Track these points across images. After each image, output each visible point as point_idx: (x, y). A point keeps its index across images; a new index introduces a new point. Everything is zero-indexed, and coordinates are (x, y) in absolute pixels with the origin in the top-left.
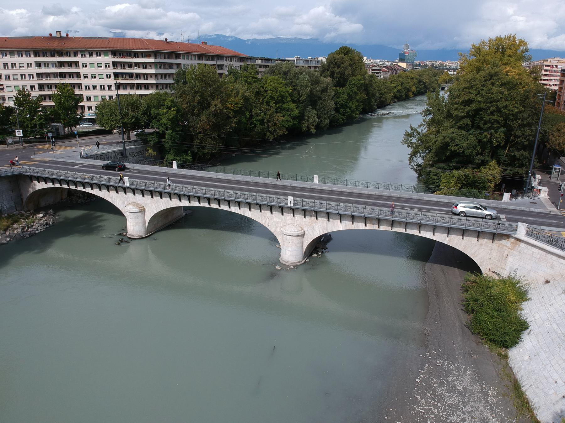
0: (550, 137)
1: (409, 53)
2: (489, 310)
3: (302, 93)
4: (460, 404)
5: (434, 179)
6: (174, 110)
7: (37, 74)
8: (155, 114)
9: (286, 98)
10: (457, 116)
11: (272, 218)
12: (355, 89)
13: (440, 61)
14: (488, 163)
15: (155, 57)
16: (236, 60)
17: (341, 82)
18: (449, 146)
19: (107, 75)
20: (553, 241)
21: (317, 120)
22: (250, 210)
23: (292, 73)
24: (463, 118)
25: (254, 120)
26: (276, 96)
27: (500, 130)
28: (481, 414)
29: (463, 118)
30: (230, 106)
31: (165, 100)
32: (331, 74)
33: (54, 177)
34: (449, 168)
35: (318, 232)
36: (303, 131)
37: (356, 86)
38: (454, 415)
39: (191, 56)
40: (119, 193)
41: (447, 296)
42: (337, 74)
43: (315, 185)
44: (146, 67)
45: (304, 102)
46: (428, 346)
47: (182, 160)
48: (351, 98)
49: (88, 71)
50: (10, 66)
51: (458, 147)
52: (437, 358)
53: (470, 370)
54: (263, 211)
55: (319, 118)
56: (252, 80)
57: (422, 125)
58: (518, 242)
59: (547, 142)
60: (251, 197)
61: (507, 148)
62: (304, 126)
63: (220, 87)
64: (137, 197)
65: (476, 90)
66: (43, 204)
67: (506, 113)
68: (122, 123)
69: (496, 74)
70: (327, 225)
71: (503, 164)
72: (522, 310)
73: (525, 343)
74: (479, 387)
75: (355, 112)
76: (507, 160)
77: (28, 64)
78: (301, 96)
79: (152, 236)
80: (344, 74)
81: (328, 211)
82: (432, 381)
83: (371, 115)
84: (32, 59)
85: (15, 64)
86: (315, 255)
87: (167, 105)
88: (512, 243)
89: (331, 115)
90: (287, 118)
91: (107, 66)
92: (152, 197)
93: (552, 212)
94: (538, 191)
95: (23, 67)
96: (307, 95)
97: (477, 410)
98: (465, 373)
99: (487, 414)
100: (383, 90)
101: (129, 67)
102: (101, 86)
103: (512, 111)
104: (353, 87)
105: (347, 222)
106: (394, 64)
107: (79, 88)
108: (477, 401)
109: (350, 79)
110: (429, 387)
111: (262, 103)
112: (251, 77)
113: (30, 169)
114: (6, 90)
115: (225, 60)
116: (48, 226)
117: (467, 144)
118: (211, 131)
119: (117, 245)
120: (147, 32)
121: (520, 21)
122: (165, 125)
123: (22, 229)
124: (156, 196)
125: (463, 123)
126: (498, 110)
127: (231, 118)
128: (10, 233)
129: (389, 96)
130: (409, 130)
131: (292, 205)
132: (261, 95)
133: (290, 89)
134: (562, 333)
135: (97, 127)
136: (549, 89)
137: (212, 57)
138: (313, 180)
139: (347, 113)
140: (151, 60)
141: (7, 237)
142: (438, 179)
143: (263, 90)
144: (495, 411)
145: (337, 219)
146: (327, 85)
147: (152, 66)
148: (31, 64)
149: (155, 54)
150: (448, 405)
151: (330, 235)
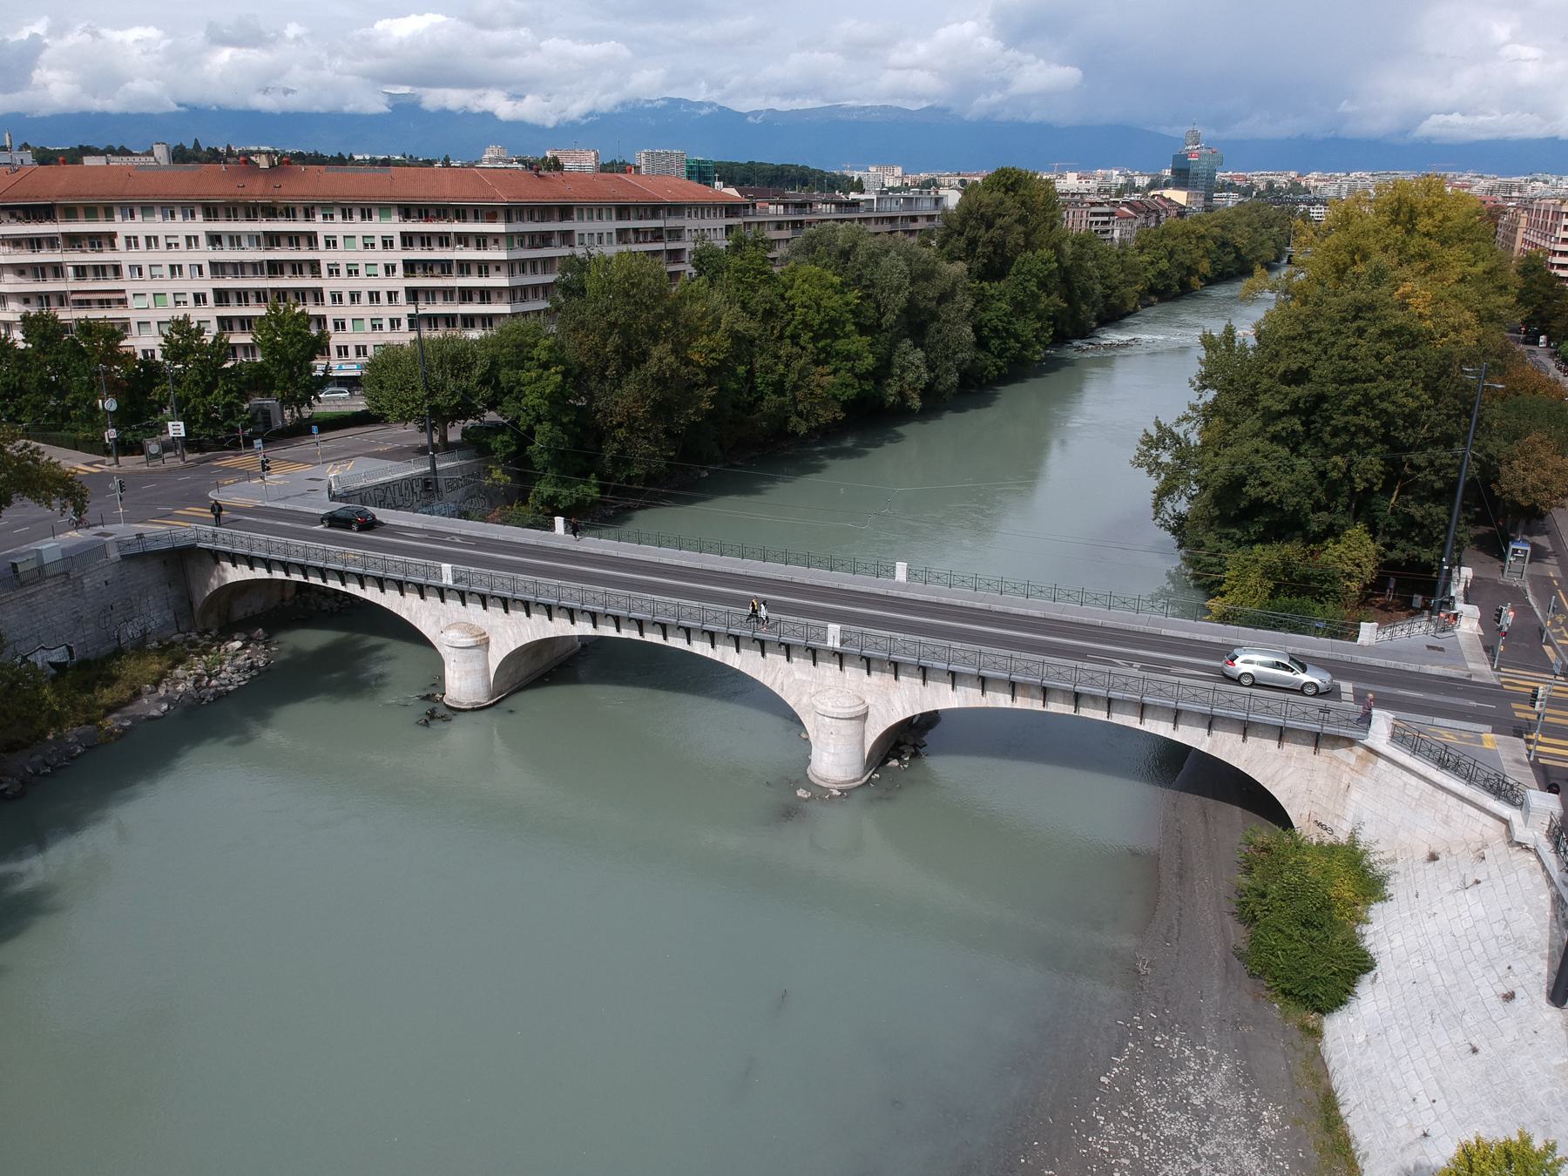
0: (1504, 469)
1: (1199, 155)
3: (886, 306)
4: (1193, 1137)
6: (557, 373)
8: (509, 382)
9: (841, 326)
10: (1267, 409)
11: (789, 673)
12: (1032, 286)
13: (1293, 174)
15: (508, 220)
16: (715, 214)
17: (995, 268)
18: (1245, 485)
19: (387, 267)
20: (1448, 760)
21: (926, 376)
22: (738, 651)
23: (861, 255)
24: (1280, 415)
30: (696, 357)
32: (968, 245)
33: (273, 556)
34: (1246, 538)
35: (900, 710)
36: (887, 405)
37: (1037, 276)
38: (1176, 1162)
40: (428, 598)
41: (1203, 879)
42: (983, 245)
44: (485, 245)
45: (891, 326)
47: (575, 496)
48: (1020, 308)
49: (339, 256)
50: (142, 242)
51: (1268, 488)
52: (1156, 1029)
53: (1229, 1062)
54: (768, 655)
55: (931, 368)
56: (755, 278)
57: (1186, 418)
58: (1372, 756)
59: (1495, 481)
61: (1396, 493)
62: (891, 392)
63: (672, 313)
64: (471, 610)
65: (1320, 341)
66: (239, 613)
67: (1385, 411)
68: (430, 407)
69: (1371, 307)
70: (921, 693)
71: (1385, 533)
73: (1361, 1002)
74: (1242, 1101)
76: (1394, 522)
77: (188, 238)
78: (884, 314)
79: (504, 704)
80: (1003, 244)
82: (1138, 1084)
84: (200, 226)
85: (156, 238)
86: (895, 763)
87: (539, 360)
88: (1359, 758)
89: (964, 360)
91: (387, 243)
92: (507, 612)
93: (1476, 675)
94: (1451, 618)
96: (900, 310)
97: (1229, 1153)
98: (1216, 1067)
99: (1251, 1162)
101: (441, 245)
102: (371, 294)
104: (1026, 281)
105: (968, 689)
106: (1152, 193)
107: (317, 300)
109: (1019, 258)
110: (1129, 1096)
111: (781, 337)
112: (754, 269)
113: (215, 536)
115: (686, 214)
116: (254, 673)
117: (1292, 482)
118: (647, 421)
119: (420, 727)
120: (481, 91)
121: (1528, 60)
122: (534, 410)
123: (196, 681)
124: (515, 609)
125: (1283, 428)
126: (1367, 401)
128: (167, 691)
129: (1131, 292)
130: (1153, 432)
131: (837, 645)
132: (777, 317)
133: (853, 296)
134: (1444, 986)
135: (359, 404)
137: (655, 210)
139: (1010, 349)
140: (499, 227)
141: (161, 700)
142: (1220, 565)
143: (782, 305)
145: (945, 681)
146: (954, 284)
148: (196, 238)
149: (509, 213)
150: (1166, 1141)
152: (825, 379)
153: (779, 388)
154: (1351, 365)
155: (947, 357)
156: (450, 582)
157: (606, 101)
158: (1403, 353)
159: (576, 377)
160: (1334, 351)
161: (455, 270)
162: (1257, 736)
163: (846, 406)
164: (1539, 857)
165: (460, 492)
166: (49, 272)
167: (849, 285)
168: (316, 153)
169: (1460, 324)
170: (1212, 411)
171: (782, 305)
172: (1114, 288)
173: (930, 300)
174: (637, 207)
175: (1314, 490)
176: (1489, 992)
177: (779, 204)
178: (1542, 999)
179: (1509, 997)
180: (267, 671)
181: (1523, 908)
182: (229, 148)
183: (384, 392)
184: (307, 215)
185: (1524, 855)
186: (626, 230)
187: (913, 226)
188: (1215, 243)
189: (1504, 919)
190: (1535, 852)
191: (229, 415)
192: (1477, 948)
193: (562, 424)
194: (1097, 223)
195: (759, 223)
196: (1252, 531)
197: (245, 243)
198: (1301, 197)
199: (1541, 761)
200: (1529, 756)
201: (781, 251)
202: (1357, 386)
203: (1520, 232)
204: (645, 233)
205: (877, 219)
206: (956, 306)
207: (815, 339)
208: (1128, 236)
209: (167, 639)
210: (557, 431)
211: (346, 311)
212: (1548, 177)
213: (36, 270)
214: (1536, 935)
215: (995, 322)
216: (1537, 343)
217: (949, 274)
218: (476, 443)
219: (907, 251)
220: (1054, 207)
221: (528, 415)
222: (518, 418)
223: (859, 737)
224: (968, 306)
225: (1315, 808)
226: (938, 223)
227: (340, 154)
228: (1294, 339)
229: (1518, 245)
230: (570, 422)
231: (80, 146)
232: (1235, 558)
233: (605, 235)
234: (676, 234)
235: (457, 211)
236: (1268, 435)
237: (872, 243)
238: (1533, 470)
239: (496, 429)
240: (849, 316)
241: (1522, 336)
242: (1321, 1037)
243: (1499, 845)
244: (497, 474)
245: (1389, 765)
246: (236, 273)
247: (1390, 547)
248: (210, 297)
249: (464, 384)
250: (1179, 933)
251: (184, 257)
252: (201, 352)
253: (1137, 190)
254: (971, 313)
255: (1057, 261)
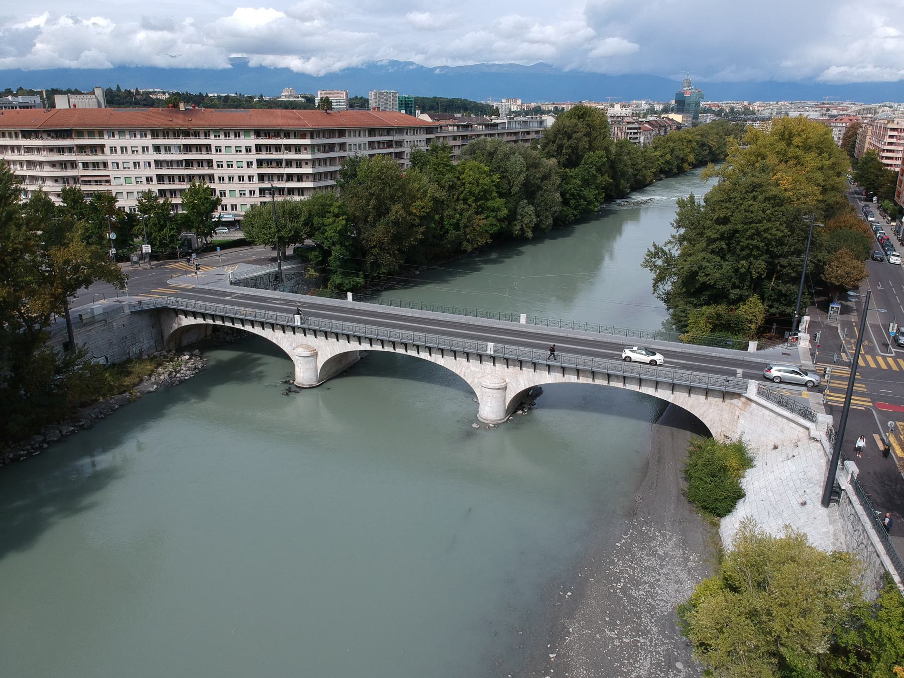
1: (691, 93)
2: (702, 476)
5: (681, 317)
6: (343, 219)
7: (155, 161)
11: (468, 367)
12: (593, 171)
14: (747, 298)
15: (312, 138)
19: (248, 163)
23: (500, 155)
24: (715, 240)
25: (446, 223)
26: (477, 190)
27: (761, 258)
28: (677, 576)
29: (715, 240)
30: (415, 211)
31: (331, 205)
35: (523, 385)
36: (514, 236)
37: (595, 165)
39: (360, 132)
42: (566, 148)
43: (522, 325)
44: (300, 151)
45: (516, 193)
46: (636, 513)
47: (352, 283)
48: (586, 183)
49: (223, 157)
50: (119, 150)
51: (709, 277)
54: (458, 359)
55: (538, 216)
57: (670, 242)
59: (823, 273)
60: (444, 341)
62: (516, 229)
67: (766, 238)
68: (278, 237)
69: (760, 186)
71: (769, 300)
72: (744, 477)
75: (593, 203)
77: (143, 148)
78: (512, 186)
80: (577, 148)
81: (534, 360)
83: (619, 204)
84: (149, 141)
86: (520, 412)
87: (333, 212)
88: (743, 403)
89: (556, 211)
90: (492, 220)
91: (248, 150)
92: (327, 339)
93: (804, 366)
94: (795, 339)
95: (137, 151)
97: (674, 572)
100: (640, 164)
101: (276, 151)
102: (239, 177)
103: (775, 235)
104: (589, 168)
105: (556, 374)
106: (662, 116)
108: (676, 565)
110: (629, 550)
111: (458, 200)
112: (443, 163)
113: (177, 302)
114: (113, 182)
116: (197, 371)
117: (720, 274)
122: (331, 239)
123: (169, 374)
124: (331, 337)
125: (717, 247)
126: (758, 233)
127: (416, 226)
129: (649, 173)
130: (652, 249)
131: (492, 353)
133: (496, 177)
135: (239, 235)
136: (890, 171)
137: (388, 131)
138: (520, 319)
139: (580, 205)
140: (307, 142)
141: (154, 383)
142: (686, 317)
143: (459, 183)
144: (692, 574)
147: (308, 149)
149: (313, 134)
150: (646, 568)
151: (541, 388)
152: (481, 222)
153: (457, 226)
154: (749, 215)
155: (546, 210)
156: (299, 324)
157: (355, 61)
158: (776, 209)
159: (352, 220)
160: (742, 207)
161: (284, 164)
162: (695, 394)
163: (492, 236)
164: (822, 444)
165: (293, 281)
166: (69, 165)
167: (493, 171)
168: (187, 93)
169: (807, 193)
170: (682, 239)
171: (459, 183)
172: (639, 171)
173: (537, 179)
174: (379, 130)
175: (732, 278)
176: (795, 502)
177: (454, 125)
178: (819, 504)
179: (804, 504)
180: (203, 370)
181: (812, 466)
182: (137, 90)
183: (254, 229)
184: (206, 136)
185: (815, 443)
186: (373, 142)
187: (528, 137)
188: (697, 144)
189: (804, 471)
190: (820, 441)
191: (172, 241)
192: (791, 484)
193: (345, 246)
194: (631, 133)
195: (444, 137)
196: (702, 299)
197: (173, 150)
198: (749, 117)
199: (829, 403)
200: (823, 401)
201: (457, 152)
202: (753, 225)
203: (868, 138)
204: (383, 143)
205: (508, 133)
206: (551, 182)
207: (476, 201)
208: (648, 141)
209: (152, 354)
210: (343, 250)
211: (226, 186)
212: (893, 104)
213: (61, 164)
214: (818, 477)
215: (573, 190)
216: (871, 201)
217: (547, 165)
218: (301, 256)
219: (525, 152)
220: (606, 127)
221: (329, 241)
222: (323, 243)
223: (503, 398)
224: (558, 182)
225: (724, 429)
226: (541, 135)
227: (200, 93)
228: (722, 201)
229: (867, 145)
230: (349, 245)
231: (52, 89)
232: (693, 313)
233: (362, 145)
234: (400, 143)
235: (285, 133)
236: (710, 250)
237: (507, 148)
238: (841, 267)
239: (310, 249)
240: (494, 188)
241: (863, 197)
242: (719, 527)
243: (805, 440)
244: (312, 272)
245: (757, 406)
246: (168, 166)
247: (771, 307)
248: (155, 179)
249: (296, 225)
250: (657, 486)
251: (141, 158)
252: (159, 209)
253: (656, 113)
254: (560, 186)
255: (607, 157)
